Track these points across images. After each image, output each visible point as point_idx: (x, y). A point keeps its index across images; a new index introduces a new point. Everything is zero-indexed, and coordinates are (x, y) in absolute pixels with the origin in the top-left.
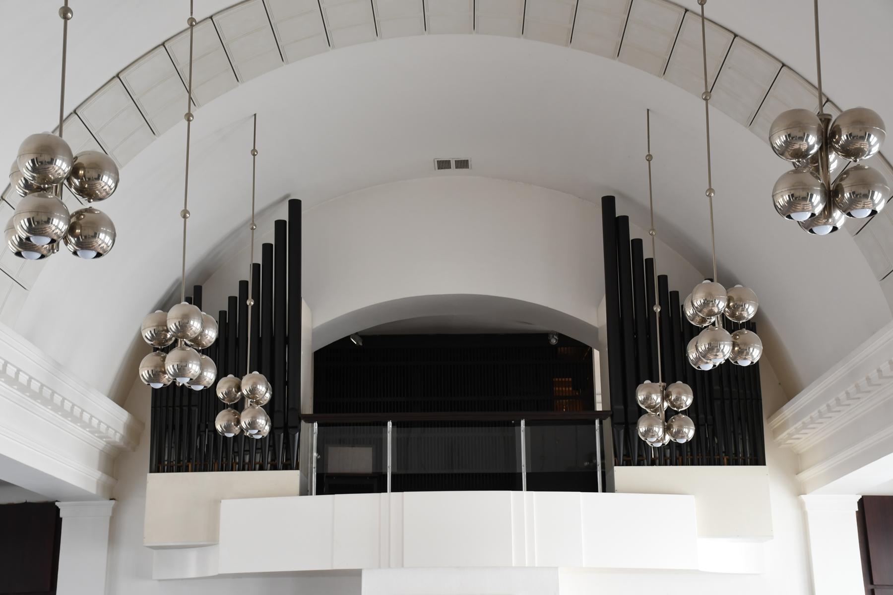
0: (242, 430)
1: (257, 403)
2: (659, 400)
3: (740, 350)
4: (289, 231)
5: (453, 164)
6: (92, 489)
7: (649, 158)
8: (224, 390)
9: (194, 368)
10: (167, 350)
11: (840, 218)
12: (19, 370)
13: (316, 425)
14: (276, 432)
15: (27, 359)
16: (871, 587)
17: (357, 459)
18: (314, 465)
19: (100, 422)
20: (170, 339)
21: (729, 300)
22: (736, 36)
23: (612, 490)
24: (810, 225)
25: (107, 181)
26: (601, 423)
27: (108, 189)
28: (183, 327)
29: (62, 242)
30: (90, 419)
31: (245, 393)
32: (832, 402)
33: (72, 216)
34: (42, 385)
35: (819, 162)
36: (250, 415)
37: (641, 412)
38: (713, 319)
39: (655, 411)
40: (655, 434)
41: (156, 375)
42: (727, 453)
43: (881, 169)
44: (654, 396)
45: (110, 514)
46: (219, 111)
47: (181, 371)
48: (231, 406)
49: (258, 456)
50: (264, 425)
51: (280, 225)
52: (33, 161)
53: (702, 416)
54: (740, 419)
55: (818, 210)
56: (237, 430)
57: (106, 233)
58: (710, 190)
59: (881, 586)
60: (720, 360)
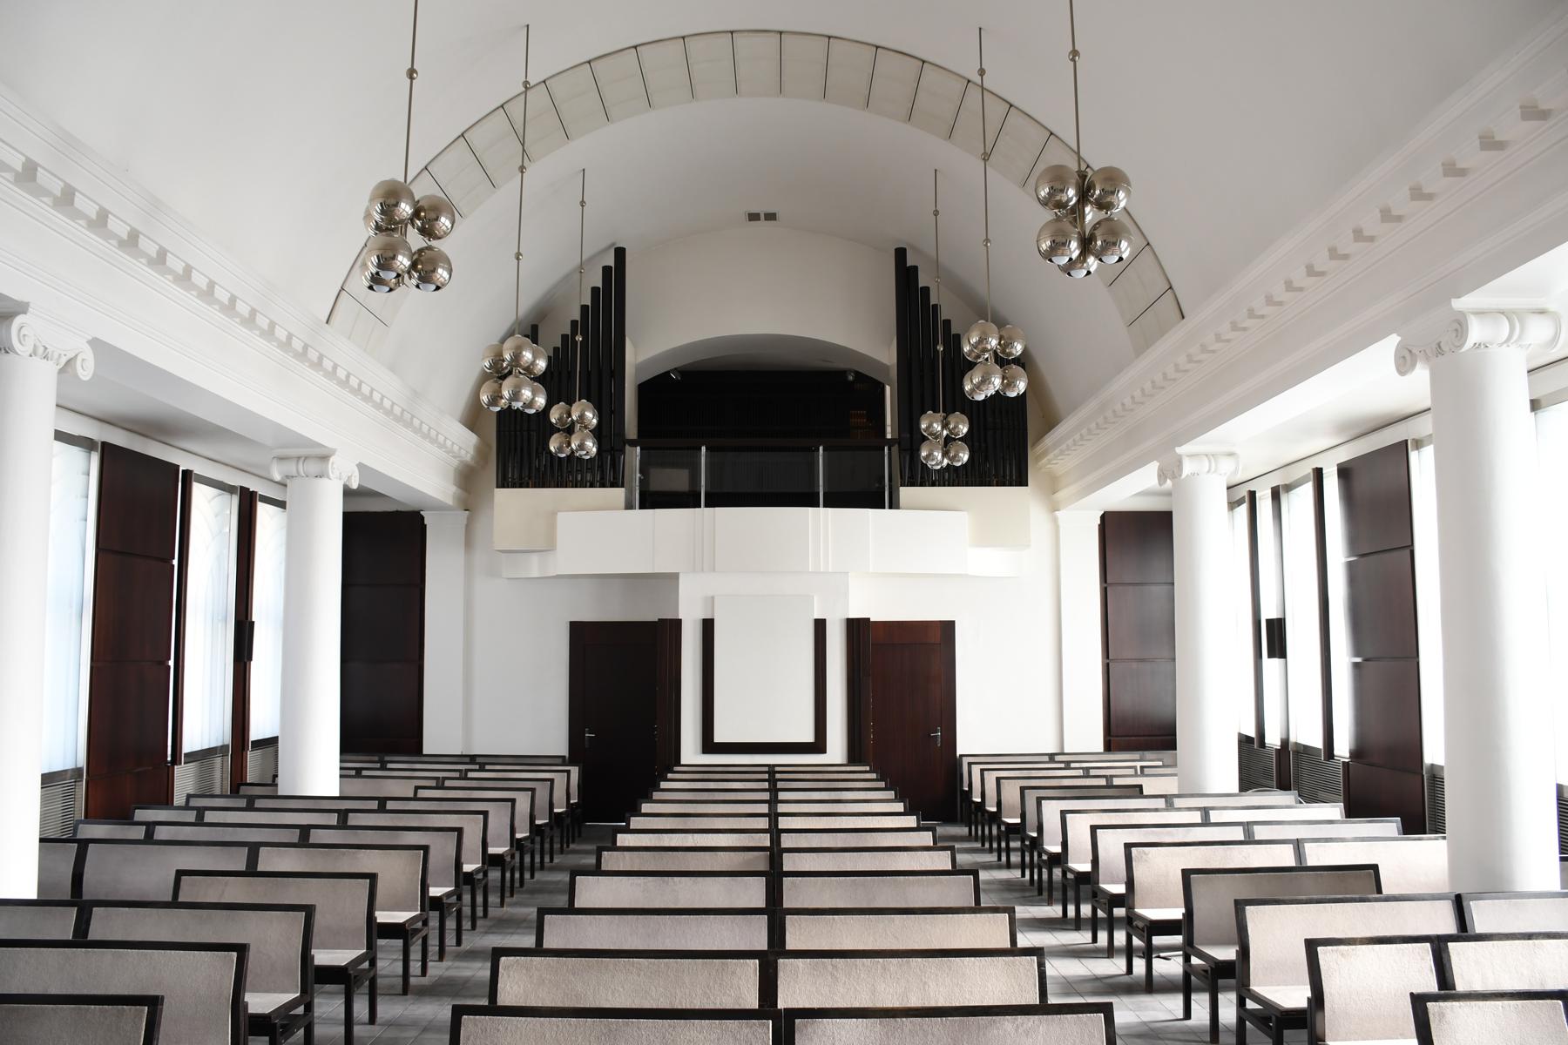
3: (1009, 382)
6: (450, 501)
7: (936, 213)
9: (527, 394)
10: (503, 377)
17: (676, 479)
23: (898, 507)
24: (1068, 269)
25: (444, 222)
32: (1084, 431)
35: (1077, 213)
37: (924, 439)
40: (936, 459)
42: (996, 476)
46: (552, 166)
47: (516, 396)
50: (591, 447)
55: (1075, 255)
56: (568, 451)
58: (987, 240)
60: (991, 392)
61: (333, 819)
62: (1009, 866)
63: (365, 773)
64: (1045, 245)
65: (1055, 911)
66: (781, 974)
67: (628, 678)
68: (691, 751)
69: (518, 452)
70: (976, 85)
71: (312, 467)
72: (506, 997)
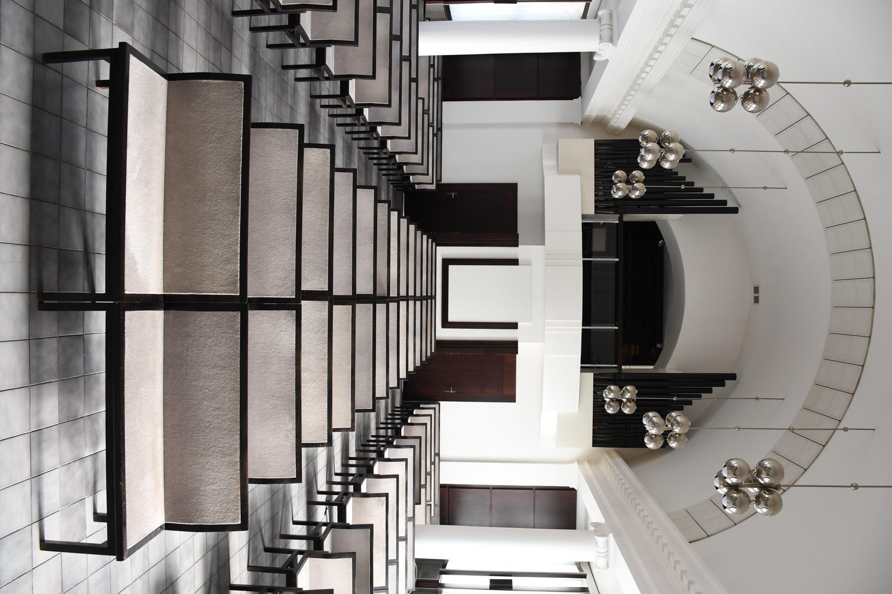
3: (653, 438)
4: (721, 208)
6: (587, 113)
7: (757, 399)
9: (649, 157)
10: (659, 143)
17: (599, 243)
24: (719, 476)
25: (753, 107)
32: (624, 481)
35: (754, 483)
37: (621, 388)
40: (609, 394)
46: (788, 168)
47: (648, 151)
50: (618, 195)
51: (725, 202)
55: (728, 480)
56: (616, 181)
58: (739, 429)
60: (648, 428)
61: (405, 53)
62: (378, 428)
63: (432, 69)
65: (353, 453)
66: (320, 302)
67: (485, 216)
68: (443, 252)
69: (615, 152)
70: (837, 426)
71: (606, 33)
72: (308, 152)
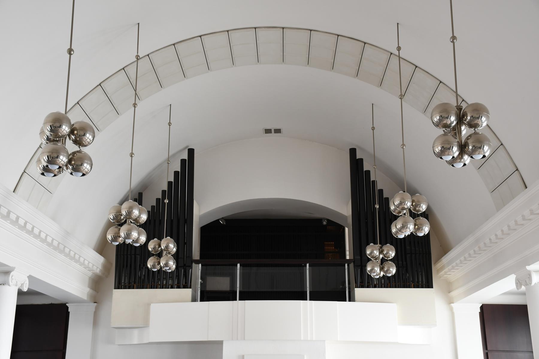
0: (161, 268)
1: (169, 253)
2: (378, 254)
3: (418, 228)
4: (188, 165)
5: (273, 131)
6: (85, 297)
7: (373, 129)
8: (152, 247)
9: (135, 235)
10: (121, 225)
11: (467, 159)
12: (47, 235)
13: (200, 265)
14: (180, 269)
15: (51, 229)
16: (486, 351)
17: (221, 283)
18: (199, 286)
19: (89, 262)
20: (123, 219)
21: (413, 201)
22: (416, 67)
23: (354, 301)
24: (452, 163)
25: (89, 136)
26: (348, 266)
27: (88, 140)
28: (129, 213)
29: (65, 168)
30: (84, 261)
31: (163, 248)
32: (467, 255)
33: (71, 154)
34: (59, 243)
35: (456, 130)
36: (165, 260)
38: (405, 212)
39: (376, 259)
41: (115, 239)
42: (413, 281)
43: (488, 134)
44: (375, 252)
45: (94, 310)
46: (152, 103)
47: (128, 236)
48: (156, 255)
49: (170, 281)
50: (172, 265)
51: (183, 161)
52: (51, 126)
53: (400, 262)
54: (420, 264)
55: (456, 154)
56: (158, 267)
57: (87, 163)
58: (403, 145)
59: (492, 351)
60: (408, 233)
64: (438, 149)
69: (129, 268)
